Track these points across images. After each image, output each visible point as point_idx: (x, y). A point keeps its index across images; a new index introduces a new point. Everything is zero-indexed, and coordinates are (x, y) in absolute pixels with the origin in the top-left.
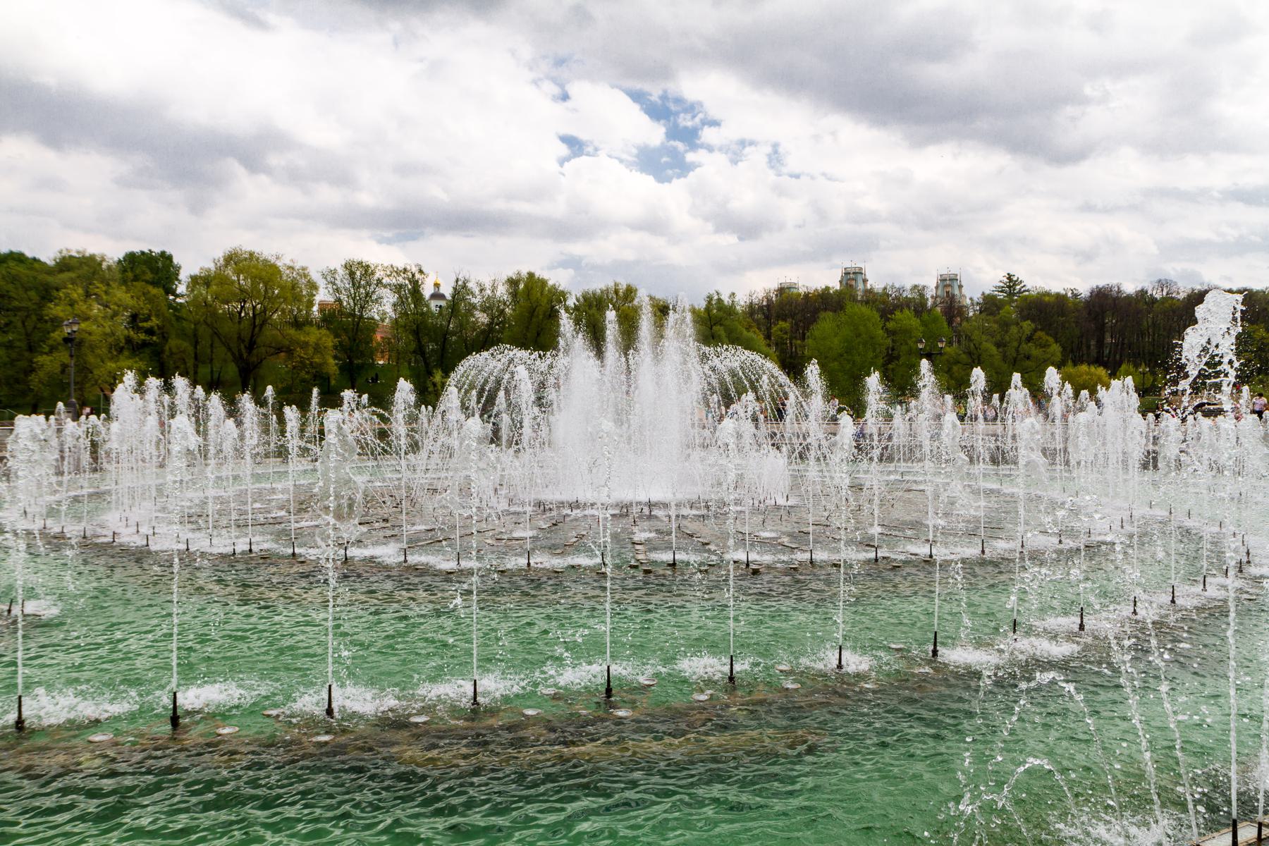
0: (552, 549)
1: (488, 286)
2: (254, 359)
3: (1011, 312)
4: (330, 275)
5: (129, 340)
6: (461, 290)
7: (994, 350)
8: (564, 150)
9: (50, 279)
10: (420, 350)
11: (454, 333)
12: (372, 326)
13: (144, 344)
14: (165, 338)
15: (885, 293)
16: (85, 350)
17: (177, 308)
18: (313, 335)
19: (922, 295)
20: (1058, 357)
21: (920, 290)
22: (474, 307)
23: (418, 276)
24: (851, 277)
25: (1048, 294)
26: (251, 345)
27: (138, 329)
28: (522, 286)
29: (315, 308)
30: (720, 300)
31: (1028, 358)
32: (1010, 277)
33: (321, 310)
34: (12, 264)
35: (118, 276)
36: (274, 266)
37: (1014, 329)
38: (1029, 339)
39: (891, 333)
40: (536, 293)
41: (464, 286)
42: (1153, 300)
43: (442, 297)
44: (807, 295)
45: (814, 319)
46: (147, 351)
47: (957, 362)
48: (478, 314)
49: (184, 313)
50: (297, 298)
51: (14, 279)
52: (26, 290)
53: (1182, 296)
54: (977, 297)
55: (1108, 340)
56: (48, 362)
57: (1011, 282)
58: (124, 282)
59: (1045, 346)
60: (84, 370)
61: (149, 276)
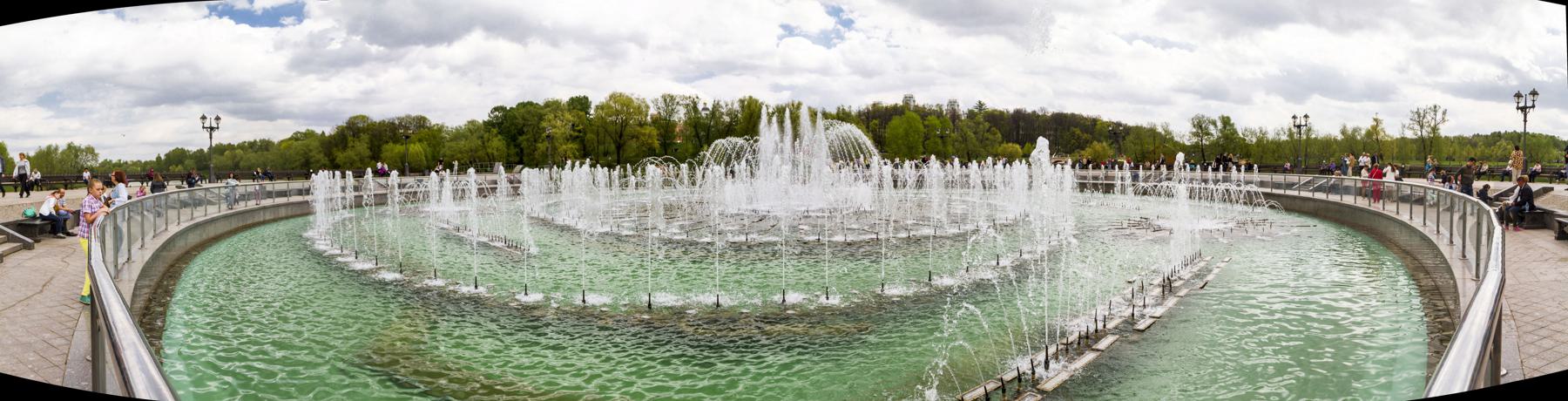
0: (760, 232)
1: (730, 103)
2: (622, 142)
3: (980, 118)
4: (655, 101)
5: (571, 136)
6: (716, 106)
7: (973, 136)
8: (781, 32)
9: (542, 111)
10: (697, 135)
11: (713, 127)
12: (674, 124)
13: (577, 137)
14: (585, 134)
15: (924, 108)
16: (555, 141)
17: (590, 121)
18: (648, 130)
19: (941, 109)
20: (1000, 139)
21: (940, 106)
22: (723, 114)
23: (696, 100)
24: (908, 99)
25: (996, 110)
26: (621, 136)
27: (574, 130)
28: (746, 103)
29: (649, 118)
30: (843, 109)
31: (987, 139)
32: (980, 102)
33: (652, 118)
34: (529, 106)
35: (567, 108)
36: (631, 99)
37: (981, 126)
38: (988, 131)
39: (925, 126)
40: (753, 106)
41: (718, 104)
42: (1039, 116)
43: (707, 109)
44: (887, 108)
45: (890, 119)
46: (578, 140)
47: (957, 141)
48: (724, 117)
49: (593, 122)
50: (641, 113)
51: (529, 112)
52: (533, 116)
53: (1049, 115)
54: (966, 111)
55: (1021, 132)
56: (542, 146)
57: (981, 105)
58: (569, 110)
59: (995, 134)
60: (555, 149)
61: (579, 107)
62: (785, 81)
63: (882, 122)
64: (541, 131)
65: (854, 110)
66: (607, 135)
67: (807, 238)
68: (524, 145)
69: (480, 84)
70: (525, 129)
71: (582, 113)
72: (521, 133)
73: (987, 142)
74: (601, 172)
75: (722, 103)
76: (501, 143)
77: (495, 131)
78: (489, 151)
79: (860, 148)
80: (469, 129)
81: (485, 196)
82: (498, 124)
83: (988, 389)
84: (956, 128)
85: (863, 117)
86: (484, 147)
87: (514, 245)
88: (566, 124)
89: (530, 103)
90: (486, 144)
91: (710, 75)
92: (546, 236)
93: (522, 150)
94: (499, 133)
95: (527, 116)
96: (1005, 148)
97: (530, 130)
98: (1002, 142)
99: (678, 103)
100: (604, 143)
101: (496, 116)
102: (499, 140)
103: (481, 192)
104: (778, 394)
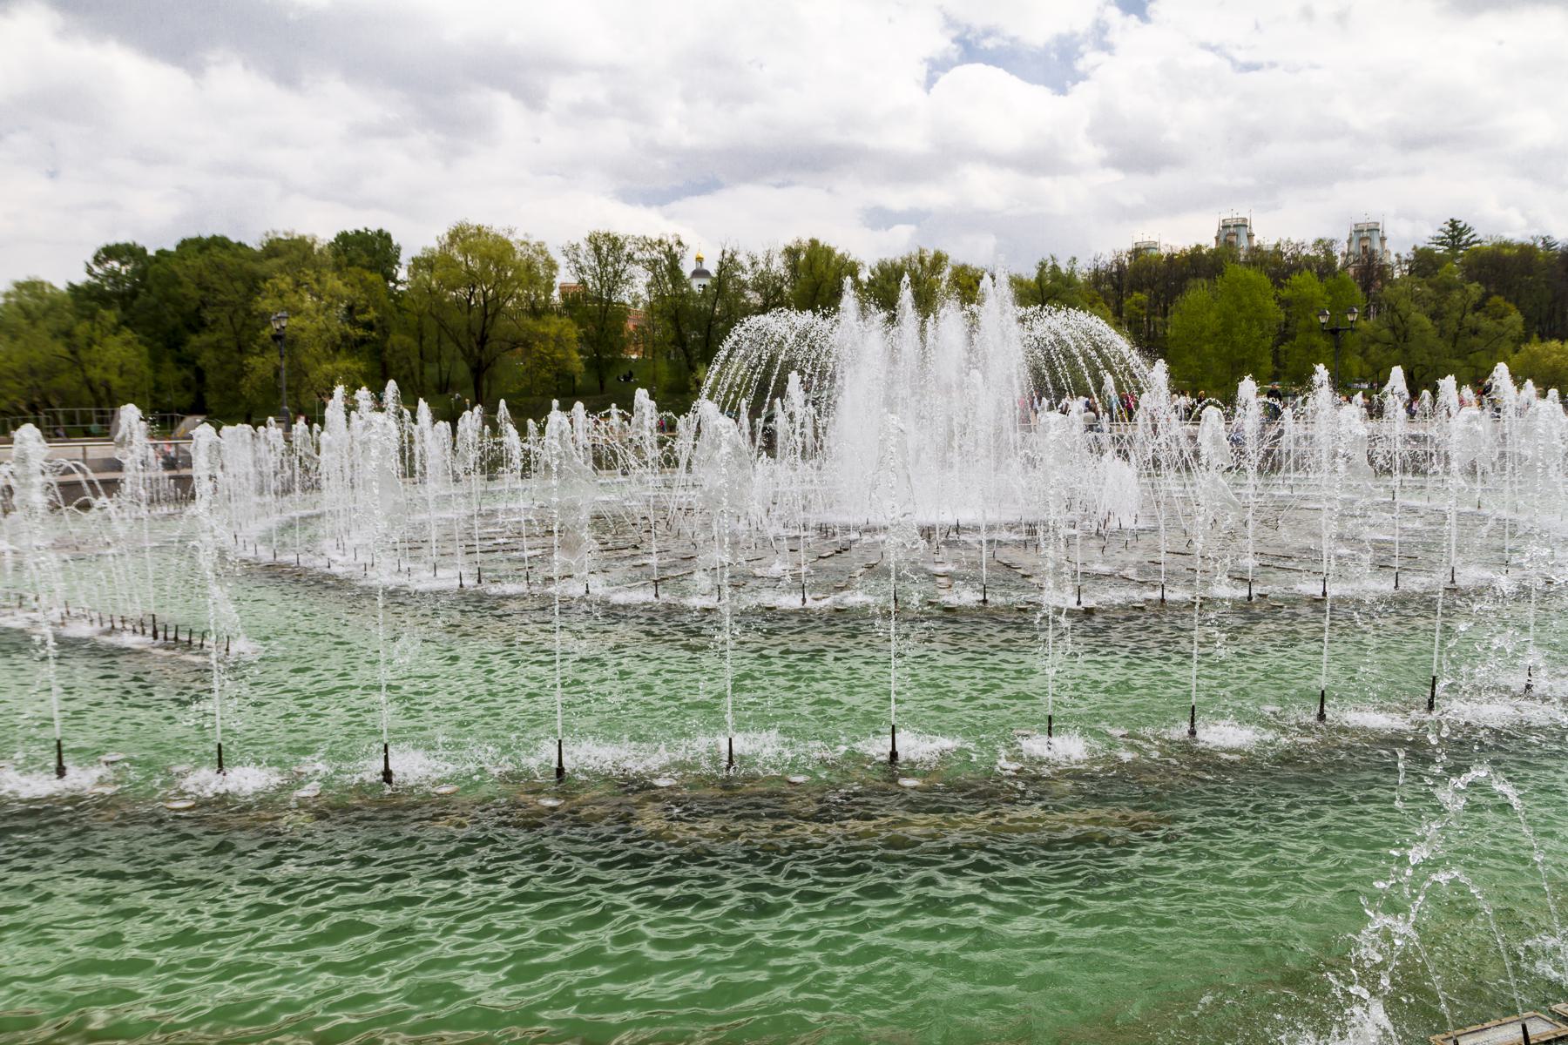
1: (761, 258)
5: (345, 337)
6: (728, 266)
7: (1427, 322)
9: (257, 267)
10: (680, 341)
12: (622, 312)
13: (363, 341)
14: (385, 332)
15: (1278, 252)
16: (298, 351)
17: (398, 298)
19: (1328, 252)
22: (744, 285)
23: (676, 249)
24: (1231, 232)
25: (1507, 245)
26: (483, 341)
27: (354, 323)
28: (803, 257)
29: (556, 294)
30: (1055, 267)
31: (1475, 332)
32: (1453, 224)
33: (563, 295)
34: (215, 250)
35: (331, 260)
36: (506, 243)
37: (1457, 295)
38: (1478, 307)
39: (1285, 303)
40: (821, 266)
41: (732, 260)
43: (705, 274)
44: (1171, 258)
46: (366, 348)
47: (1375, 341)
48: (750, 294)
49: (405, 304)
50: (533, 281)
51: (219, 268)
52: (232, 280)
54: (1407, 252)
56: (260, 365)
57: (1456, 231)
58: (338, 268)
60: (299, 372)
61: (365, 259)
62: (896, 199)
63: (1157, 296)
64: (258, 322)
65: (1083, 269)
66: (445, 337)
67: (951, 598)
68: (207, 359)
69: (53, 175)
70: (208, 316)
71: (372, 277)
72: (196, 324)
73: (1474, 339)
74: (430, 433)
75: (741, 258)
76: (131, 352)
77: (111, 316)
78: (95, 373)
79: (1101, 358)
80: (20, 306)
81: (86, 506)
82: (121, 296)
83: (1531, 1032)
84: (1374, 303)
85: (1108, 287)
86: (77, 363)
87: (184, 637)
88: (329, 306)
89: (220, 243)
90: (83, 354)
91: (707, 186)
92: (274, 606)
93: (200, 374)
94: (126, 323)
95: (213, 279)
96: (1534, 356)
97: (224, 318)
98: (1526, 339)
99: (630, 257)
100: (439, 358)
101: (114, 274)
102: (127, 343)
103: (71, 494)
104: (886, 991)
